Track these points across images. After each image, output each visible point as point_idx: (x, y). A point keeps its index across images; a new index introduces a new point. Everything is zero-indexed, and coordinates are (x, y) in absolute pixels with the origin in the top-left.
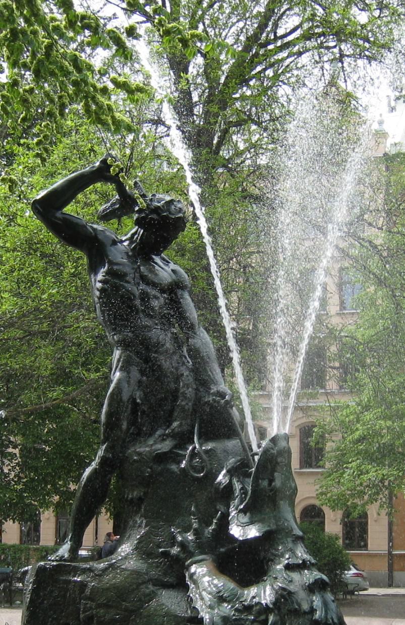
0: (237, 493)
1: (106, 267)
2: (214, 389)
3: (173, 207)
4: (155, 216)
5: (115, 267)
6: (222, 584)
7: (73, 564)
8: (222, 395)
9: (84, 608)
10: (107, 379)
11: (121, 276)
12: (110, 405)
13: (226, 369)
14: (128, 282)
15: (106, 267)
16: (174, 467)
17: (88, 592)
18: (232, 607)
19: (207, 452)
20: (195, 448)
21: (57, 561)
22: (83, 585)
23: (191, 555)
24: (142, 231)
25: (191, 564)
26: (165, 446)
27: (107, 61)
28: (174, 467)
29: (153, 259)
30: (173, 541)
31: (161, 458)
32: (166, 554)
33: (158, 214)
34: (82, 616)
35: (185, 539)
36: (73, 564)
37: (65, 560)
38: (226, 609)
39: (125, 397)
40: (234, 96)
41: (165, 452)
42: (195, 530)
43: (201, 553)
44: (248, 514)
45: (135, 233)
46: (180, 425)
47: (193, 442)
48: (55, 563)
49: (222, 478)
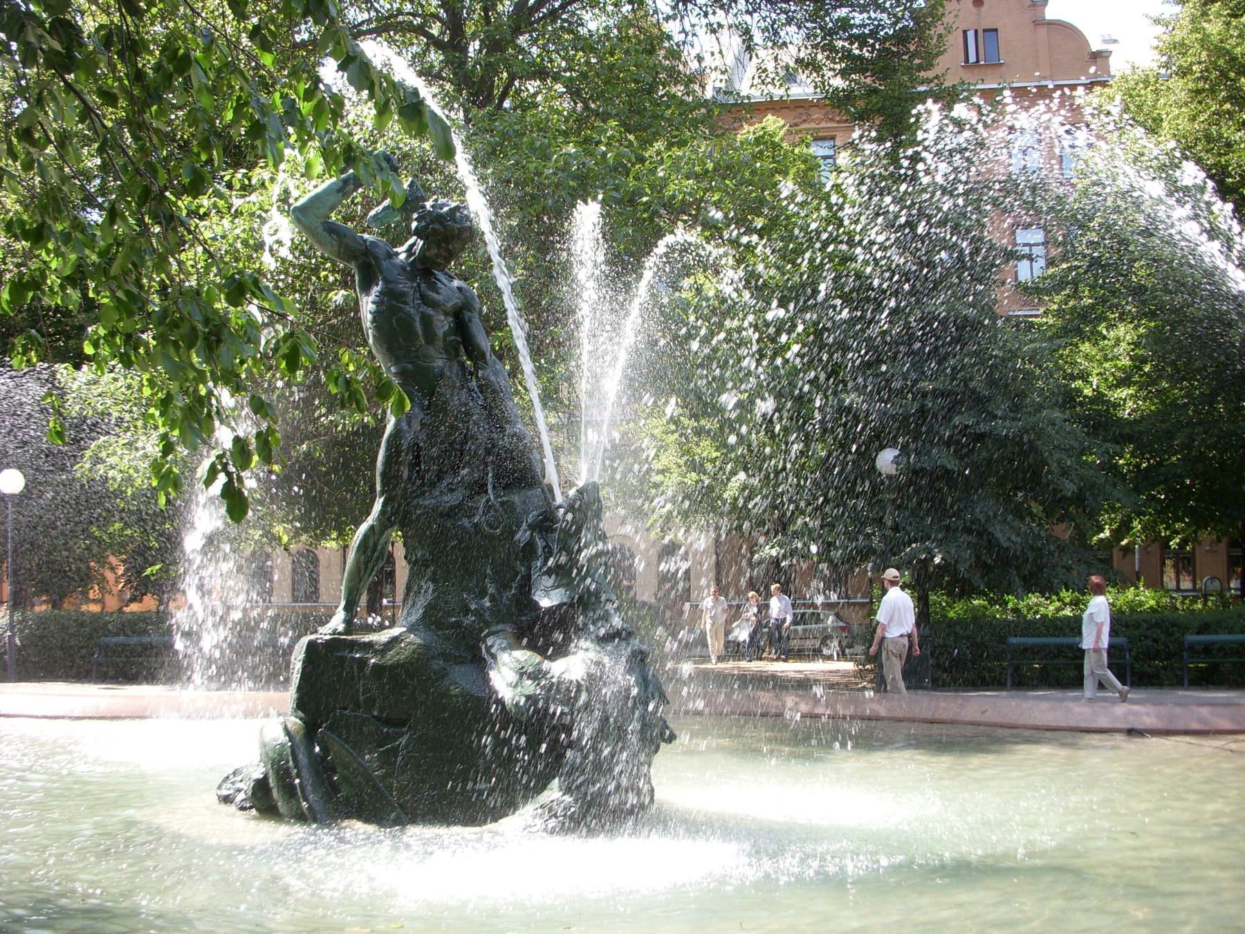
0: (540, 551)
4: (437, 226)
8: (520, 438)
10: (382, 422)
12: (388, 449)
13: (930, 116)
14: (406, 303)
16: (466, 522)
17: (368, 671)
19: (502, 504)
23: (488, 624)
24: (421, 243)
25: (488, 635)
26: (451, 499)
30: (466, 611)
31: (452, 513)
32: (458, 625)
33: (441, 223)
34: (362, 698)
37: (340, 634)
38: (529, 687)
39: (408, 438)
40: (587, 218)
42: (492, 596)
45: (414, 244)
48: (328, 637)
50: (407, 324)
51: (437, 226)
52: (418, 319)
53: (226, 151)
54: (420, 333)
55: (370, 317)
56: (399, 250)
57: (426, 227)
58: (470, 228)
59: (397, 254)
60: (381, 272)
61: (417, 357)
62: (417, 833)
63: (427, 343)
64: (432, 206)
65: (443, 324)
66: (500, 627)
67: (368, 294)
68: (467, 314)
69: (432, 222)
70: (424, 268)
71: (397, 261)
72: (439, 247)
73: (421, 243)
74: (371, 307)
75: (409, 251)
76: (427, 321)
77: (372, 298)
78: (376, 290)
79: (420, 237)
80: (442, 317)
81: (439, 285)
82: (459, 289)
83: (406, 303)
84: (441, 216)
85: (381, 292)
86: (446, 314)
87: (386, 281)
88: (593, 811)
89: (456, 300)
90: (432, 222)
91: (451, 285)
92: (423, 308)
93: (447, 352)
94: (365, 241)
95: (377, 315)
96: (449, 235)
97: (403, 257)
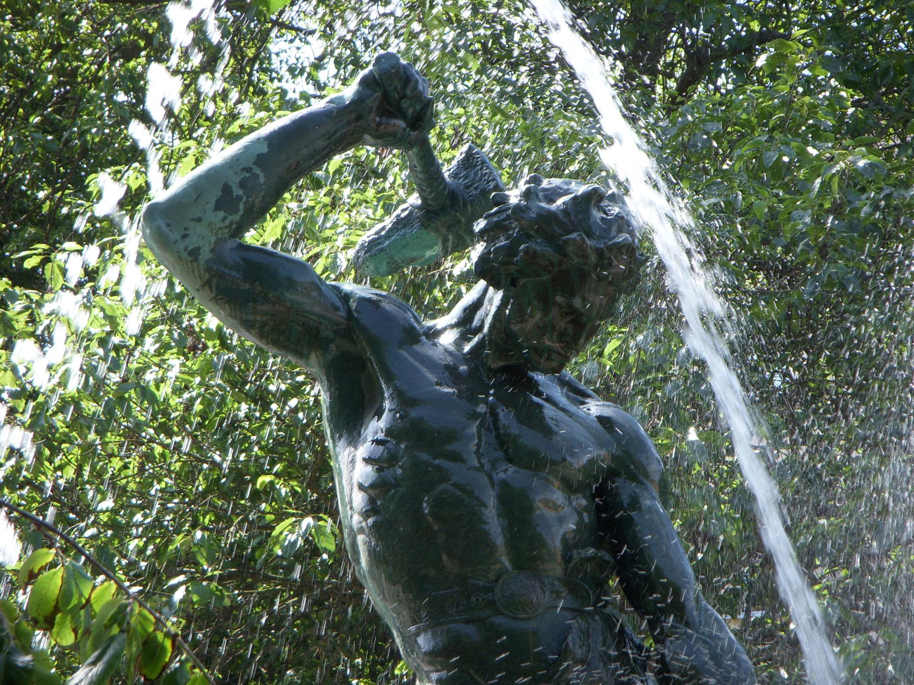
4: (539, 246)
14: (456, 457)
24: (496, 297)
33: (551, 239)
45: (477, 305)
50: (459, 513)
51: (539, 246)
52: (491, 499)
53: (232, 369)
54: (499, 541)
55: (359, 499)
56: (440, 322)
57: (511, 250)
58: (629, 249)
59: (437, 333)
60: (390, 378)
61: (491, 604)
62: (470, 303)
63: (518, 565)
64: (527, 195)
65: (561, 516)
67: (354, 440)
68: (624, 488)
69: (526, 236)
70: (507, 365)
71: (436, 354)
72: (545, 300)
73: (496, 297)
74: (363, 472)
75: (466, 323)
76: (516, 507)
77: (364, 450)
78: (376, 427)
79: (494, 282)
80: (558, 497)
81: (549, 411)
82: (603, 420)
83: (456, 457)
84: (550, 216)
85: (389, 432)
86: (569, 487)
87: (404, 401)
88: (302, 245)
89: (590, 453)
90: (526, 236)
91: (581, 408)
92: (508, 472)
93: (573, 589)
94: (346, 297)
95: (378, 492)
96: (570, 269)
97: (448, 339)
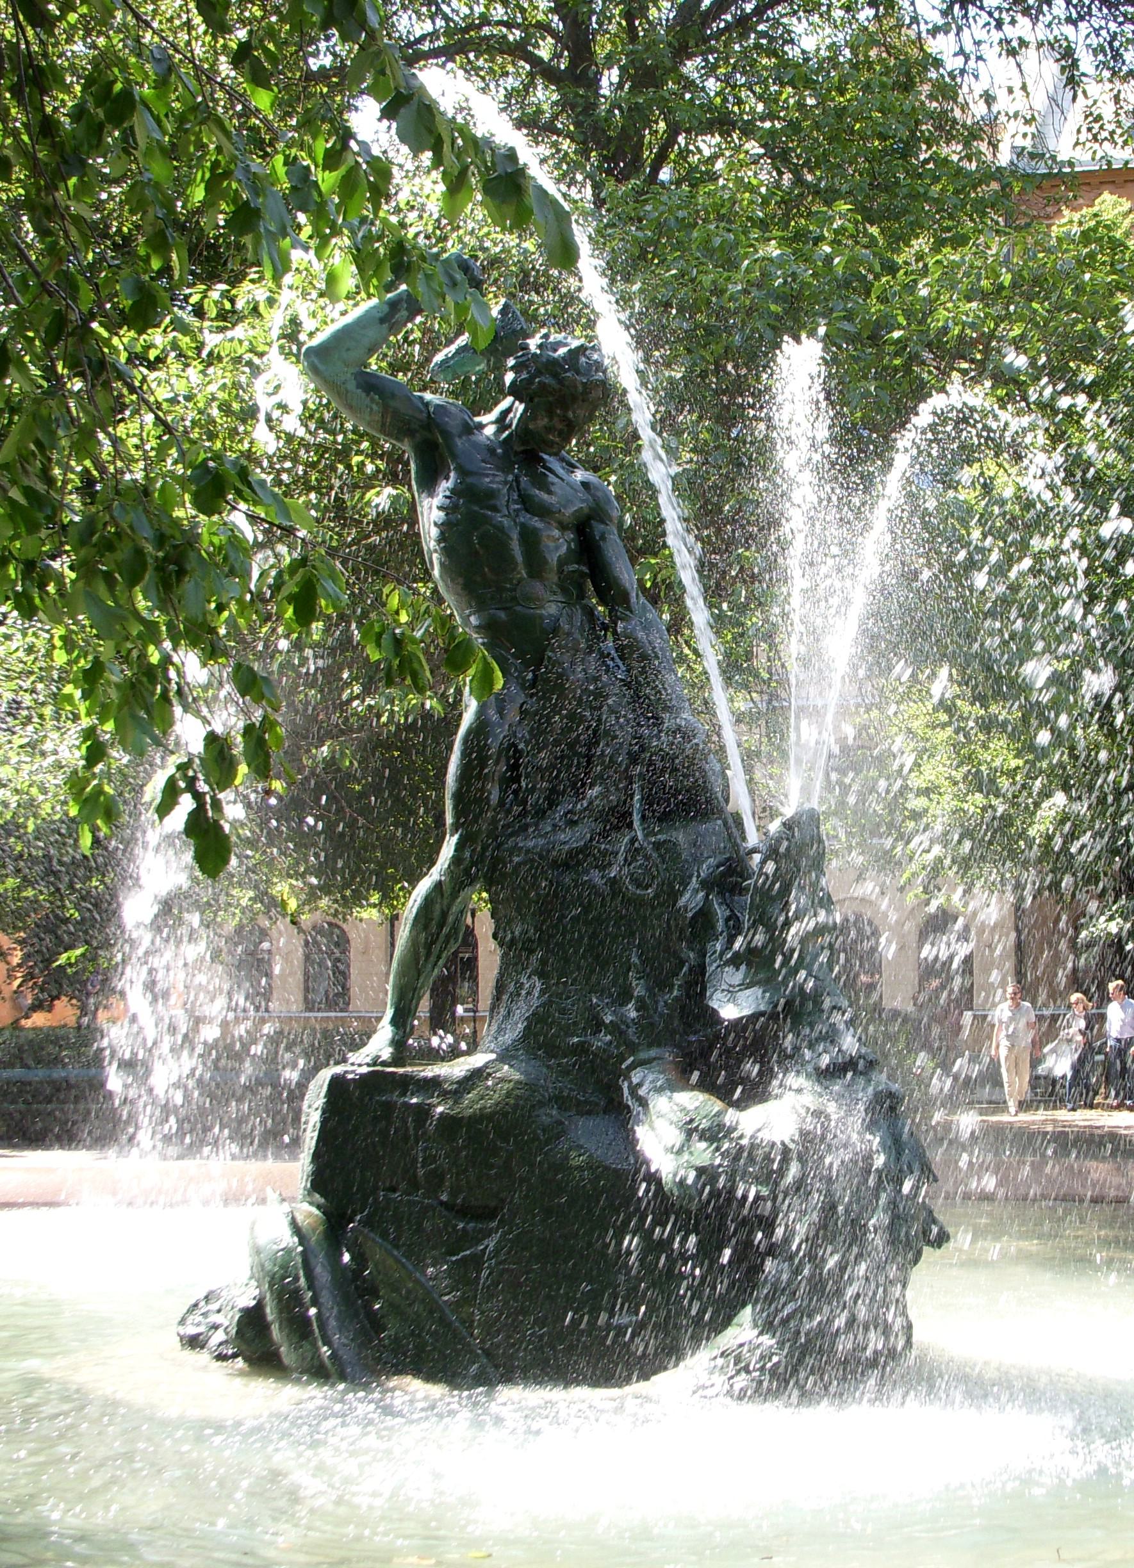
1: (451, 480)
2: (668, 723)
3: (583, 359)
4: (548, 380)
5: (469, 480)
6: (682, 902)
7: (401, 1070)
9: (425, 1159)
10: (454, 708)
11: (485, 498)
12: (465, 754)
14: (495, 509)
15: (451, 480)
18: (717, 1149)
19: (657, 846)
20: (633, 840)
21: (368, 1065)
22: (423, 1112)
23: (633, 1048)
26: (571, 838)
27: (1004, 1399)
28: (596, 877)
29: (542, 460)
30: (597, 1025)
31: (573, 861)
33: (555, 376)
34: (421, 1172)
35: (623, 1020)
36: (401, 1070)
37: (384, 1064)
39: (501, 733)
41: (417, 1372)
43: (650, 1046)
44: (743, 967)
45: (509, 410)
46: (604, 795)
47: (630, 826)
49: (691, 899)
66: (653, 1053)
